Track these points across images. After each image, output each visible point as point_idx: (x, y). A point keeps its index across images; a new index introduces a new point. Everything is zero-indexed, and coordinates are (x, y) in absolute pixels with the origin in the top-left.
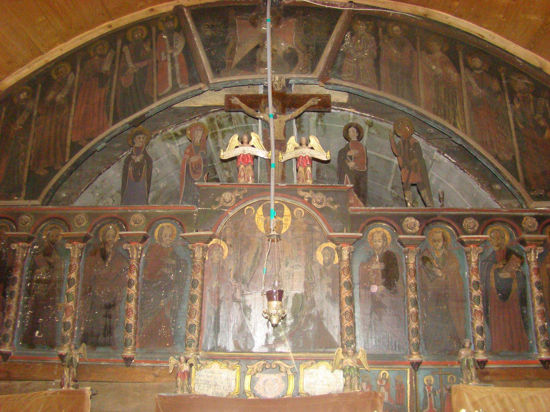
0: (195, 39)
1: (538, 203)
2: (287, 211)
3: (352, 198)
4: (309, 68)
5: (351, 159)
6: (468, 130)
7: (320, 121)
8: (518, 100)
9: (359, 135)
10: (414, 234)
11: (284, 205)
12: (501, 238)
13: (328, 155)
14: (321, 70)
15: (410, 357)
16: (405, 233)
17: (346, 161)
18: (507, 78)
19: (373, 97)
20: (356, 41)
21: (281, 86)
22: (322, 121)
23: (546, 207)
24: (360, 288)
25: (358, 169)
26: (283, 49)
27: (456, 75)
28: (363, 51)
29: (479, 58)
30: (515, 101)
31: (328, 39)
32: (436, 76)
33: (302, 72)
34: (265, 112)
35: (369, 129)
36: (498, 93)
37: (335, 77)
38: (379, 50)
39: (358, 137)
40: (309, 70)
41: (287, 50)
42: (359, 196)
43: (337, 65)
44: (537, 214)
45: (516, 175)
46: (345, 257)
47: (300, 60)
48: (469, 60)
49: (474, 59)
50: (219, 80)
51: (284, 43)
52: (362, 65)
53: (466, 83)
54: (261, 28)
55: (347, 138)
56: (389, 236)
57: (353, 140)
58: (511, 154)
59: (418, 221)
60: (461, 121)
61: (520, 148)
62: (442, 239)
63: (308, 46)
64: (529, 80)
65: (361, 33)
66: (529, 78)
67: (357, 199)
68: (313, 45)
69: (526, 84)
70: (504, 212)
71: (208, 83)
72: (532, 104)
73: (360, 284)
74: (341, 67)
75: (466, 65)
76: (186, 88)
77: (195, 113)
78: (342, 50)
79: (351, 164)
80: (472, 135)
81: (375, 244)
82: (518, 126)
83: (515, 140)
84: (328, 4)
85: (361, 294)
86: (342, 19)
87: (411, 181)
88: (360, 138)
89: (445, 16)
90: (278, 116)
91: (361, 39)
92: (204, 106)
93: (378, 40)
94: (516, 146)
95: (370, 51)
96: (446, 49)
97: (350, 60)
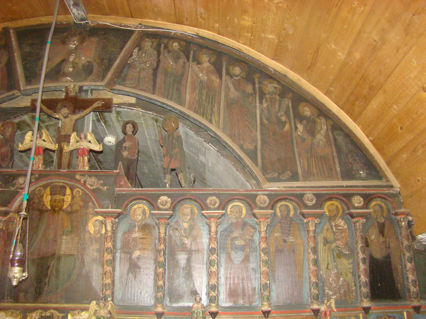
0: (16, 54)
1: (272, 184)
2: (68, 191)
3: (123, 180)
4: (101, 77)
5: (126, 149)
6: (221, 125)
7: (119, 117)
8: (266, 101)
9: (134, 130)
10: (166, 210)
11: (66, 186)
12: (239, 213)
13: (101, 147)
14: (108, 78)
15: (155, 309)
16: (160, 209)
17: (121, 151)
18: (260, 83)
19: (147, 99)
20: (142, 54)
21: (75, 92)
22: (121, 117)
23: (277, 187)
24: (121, 252)
25: (130, 157)
26: (83, 62)
27: (218, 80)
28: (145, 63)
29: (239, 67)
30: (264, 101)
31: (119, 54)
32: (201, 82)
33: (94, 81)
34: (61, 112)
35: (156, 124)
36: (251, 95)
37: (119, 84)
38: (158, 62)
39: (133, 132)
40: (100, 79)
41: (86, 62)
42: (128, 179)
43: (123, 74)
44: (269, 192)
45: (256, 162)
46: (109, 228)
47: (95, 71)
48: (231, 68)
49: (235, 68)
50: (29, 87)
51: (85, 57)
52: (143, 73)
53: (225, 87)
54: (69, 45)
55: (125, 133)
56: (148, 211)
57: (128, 134)
58: (254, 145)
59: (363, 198)
60: (216, 118)
61: (262, 139)
62: (190, 213)
63: (102, 60)
64: (278, 85)
65: (147, 49)
66: (278, 82)
67: (127, 181)
68: (106, 59)
69: (275, 88)
70: (241, 191)
71: (19, 90)
72: (277, 103)
73: (121, 249)
74: (126, 75)
75: (228, 73)
76: (4, 93)
77: (19, 112)
78: (129, 62)
79: (125, 154)
80: (224, 130)
81: (136, 217)
82: (263, 121)
83: (259, 132)
84: (124, 26)
85: (121, 257)
86: (133, 37)
87: (171, 167)
88: (135, 132)
89: (212, 34)
90: (70, 115)
91: (145, 53)
92: (25, 107)
93: (159, 54)
94: (259, 137)
95: (151, 63)
96: (213, 60)
97: (134, 70)
